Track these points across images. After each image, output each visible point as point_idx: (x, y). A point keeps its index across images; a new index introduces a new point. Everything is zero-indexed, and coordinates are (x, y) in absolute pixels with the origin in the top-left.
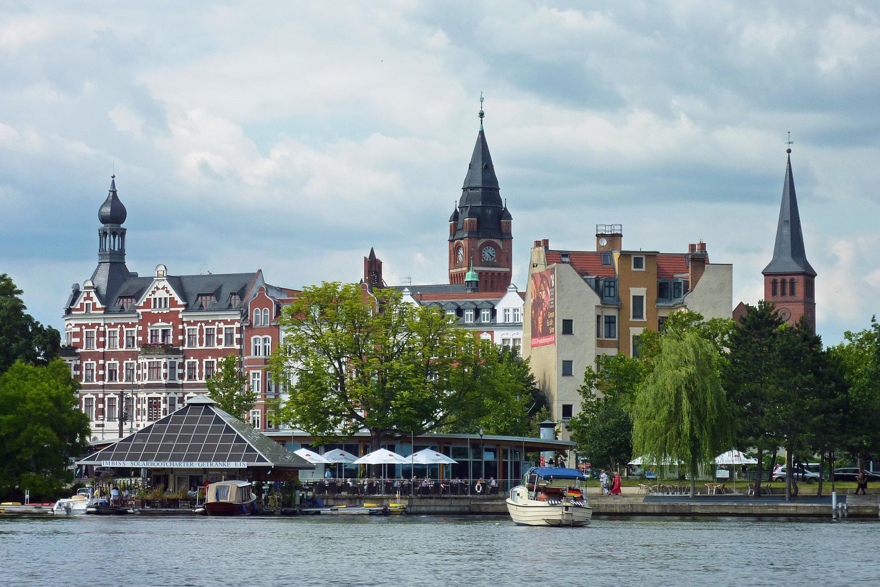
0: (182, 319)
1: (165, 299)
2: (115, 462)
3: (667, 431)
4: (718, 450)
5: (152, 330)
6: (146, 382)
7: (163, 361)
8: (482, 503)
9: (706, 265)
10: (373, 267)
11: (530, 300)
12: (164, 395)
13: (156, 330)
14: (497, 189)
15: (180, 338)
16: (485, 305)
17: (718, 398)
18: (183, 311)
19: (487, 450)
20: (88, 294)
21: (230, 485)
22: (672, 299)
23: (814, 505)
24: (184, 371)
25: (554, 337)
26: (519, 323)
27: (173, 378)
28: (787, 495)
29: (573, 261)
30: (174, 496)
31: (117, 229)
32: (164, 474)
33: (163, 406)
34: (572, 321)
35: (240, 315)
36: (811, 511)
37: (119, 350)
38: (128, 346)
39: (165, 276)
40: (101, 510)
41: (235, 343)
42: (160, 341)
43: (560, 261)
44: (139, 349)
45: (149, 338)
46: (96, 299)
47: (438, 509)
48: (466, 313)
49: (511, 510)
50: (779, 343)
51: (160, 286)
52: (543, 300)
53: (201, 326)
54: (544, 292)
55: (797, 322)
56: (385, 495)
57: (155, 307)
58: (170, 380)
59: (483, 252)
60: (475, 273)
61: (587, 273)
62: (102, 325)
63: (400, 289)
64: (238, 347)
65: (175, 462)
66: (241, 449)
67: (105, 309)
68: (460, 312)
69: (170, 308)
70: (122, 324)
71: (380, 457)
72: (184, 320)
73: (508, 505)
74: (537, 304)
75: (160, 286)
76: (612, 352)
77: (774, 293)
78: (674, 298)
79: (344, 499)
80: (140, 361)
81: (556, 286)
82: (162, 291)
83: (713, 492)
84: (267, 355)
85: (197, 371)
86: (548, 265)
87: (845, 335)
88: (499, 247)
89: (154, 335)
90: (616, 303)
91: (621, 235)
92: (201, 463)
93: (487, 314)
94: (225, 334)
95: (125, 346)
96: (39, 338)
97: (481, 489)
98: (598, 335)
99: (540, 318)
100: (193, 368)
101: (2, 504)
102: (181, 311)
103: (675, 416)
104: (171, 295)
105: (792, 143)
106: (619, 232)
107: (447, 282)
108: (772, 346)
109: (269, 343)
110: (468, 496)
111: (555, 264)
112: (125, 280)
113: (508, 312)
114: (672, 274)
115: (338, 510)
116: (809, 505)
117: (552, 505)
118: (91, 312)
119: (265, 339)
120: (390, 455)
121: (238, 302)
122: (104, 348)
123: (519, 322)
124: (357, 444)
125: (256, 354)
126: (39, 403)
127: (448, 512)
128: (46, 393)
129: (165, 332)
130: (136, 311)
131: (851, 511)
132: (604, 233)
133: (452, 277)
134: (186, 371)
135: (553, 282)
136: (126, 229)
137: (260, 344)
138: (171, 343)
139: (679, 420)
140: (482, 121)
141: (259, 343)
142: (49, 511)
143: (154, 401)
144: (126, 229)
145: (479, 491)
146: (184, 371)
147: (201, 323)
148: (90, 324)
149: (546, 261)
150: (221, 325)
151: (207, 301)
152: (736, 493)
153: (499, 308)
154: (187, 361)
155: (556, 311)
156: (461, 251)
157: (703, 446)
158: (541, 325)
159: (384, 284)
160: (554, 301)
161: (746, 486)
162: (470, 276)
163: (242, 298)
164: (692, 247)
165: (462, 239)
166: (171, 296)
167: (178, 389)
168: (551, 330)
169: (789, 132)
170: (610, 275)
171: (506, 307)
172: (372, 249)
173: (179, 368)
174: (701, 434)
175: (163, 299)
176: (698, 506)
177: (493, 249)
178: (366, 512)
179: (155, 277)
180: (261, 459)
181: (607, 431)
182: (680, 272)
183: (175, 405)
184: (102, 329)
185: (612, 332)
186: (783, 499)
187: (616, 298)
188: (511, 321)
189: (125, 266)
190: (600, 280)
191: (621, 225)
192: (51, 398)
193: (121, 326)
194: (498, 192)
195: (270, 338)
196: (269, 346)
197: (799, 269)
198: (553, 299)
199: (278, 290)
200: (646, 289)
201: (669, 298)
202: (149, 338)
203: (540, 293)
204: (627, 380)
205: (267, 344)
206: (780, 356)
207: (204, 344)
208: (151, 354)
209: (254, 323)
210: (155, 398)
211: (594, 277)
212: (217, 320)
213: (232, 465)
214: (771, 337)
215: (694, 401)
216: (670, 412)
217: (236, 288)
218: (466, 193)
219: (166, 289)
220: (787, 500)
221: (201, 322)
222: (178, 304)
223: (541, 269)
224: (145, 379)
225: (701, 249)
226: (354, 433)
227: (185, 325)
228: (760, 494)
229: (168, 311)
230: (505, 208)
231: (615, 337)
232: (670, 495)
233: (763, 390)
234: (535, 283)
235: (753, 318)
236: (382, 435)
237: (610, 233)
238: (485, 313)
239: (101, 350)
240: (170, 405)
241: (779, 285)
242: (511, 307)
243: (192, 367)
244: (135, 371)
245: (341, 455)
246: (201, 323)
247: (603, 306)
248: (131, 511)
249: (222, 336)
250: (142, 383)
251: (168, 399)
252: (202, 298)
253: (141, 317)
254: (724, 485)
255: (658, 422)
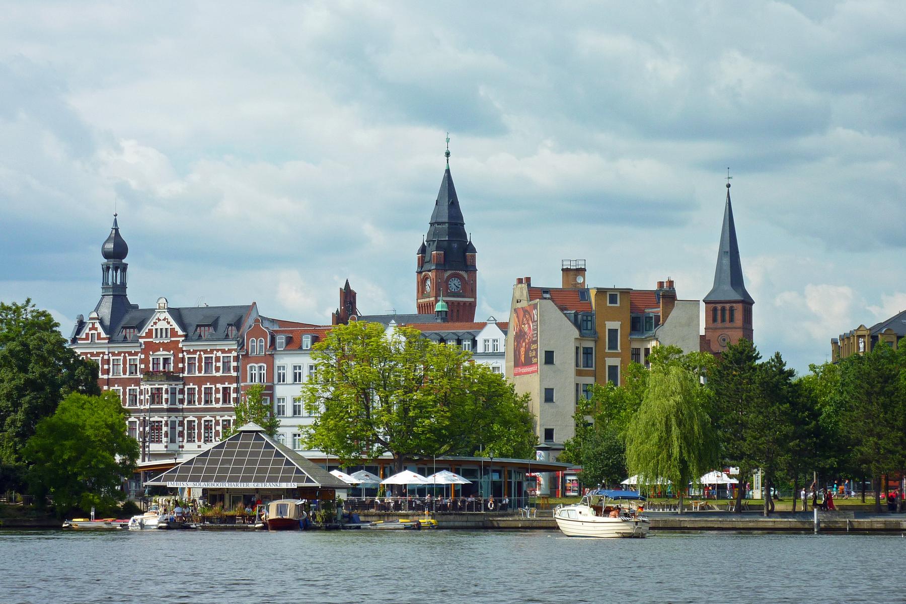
0: (182, 348)
1: (166, 329)
2: (179, 483)
3: (658, 455)
4: (703, 471)
5: (153, 359)
6: (147, 407)
7: (165, 387)
8: (495, 519)
9: (676, 302)
10: (348, 297)
11: (512, 333)
12: (165, 418)
13: (157, 358)
14: (463, 224)
15: (180, 365)
16: (466, 336)
17: (703, 425)
18: (183, 341)
19: (494, 471)
20: (93, 324)
21: (289, 503)
22: (644, 332)
23: (790, 520)
24: (184, 397)
25: (536, 367)
26: (498, 353)
27: (173, 403)
28: (765, 511)
29: (553, 297)
30: (232, 513)
31: (119, 264)
32: (221, 493)
33: (164, 429)
34: (553, 352)
35: (236, 345)
36: (787, 526)
37: (123, 376)
38: (131, 373)
39: (166, 308)
40: (171, 525)
41: (232, 371)
42: (161, 368)
43: (541, 297)
44: (142, 376)
45: (151, 365)
46: (100, 330)
47: (457, 524)
48: (464, 343)
49: (560, 523)
50: (758, 376)
51: (162, 318)
52: (525, 333)
53: (200, 355)
54: (526, 326)
55: (773, 358)
56: (409, 512)
57: (156, 337)
58: (171, 404)
59: (450, 283)
60: (444, 303)
61: (566, 308)
62: (107, 353)
63: (385, 320)
64: (235, 374)
65: (232, 483)
66: (291, 471)
67: (109, 339)
68: (459, 342)
69: (171, 337)
70: (125, 353)
71: (406, 477)
72: (184, 349)
73: (557, 519)
74: (520, 336)
75: (162, 318)
76: (590, 380)
77: (715, 320)
78: (646, 330)
79: (374, 516)
80: (142, 387)
81: (539, 321)
82: (163, 322)
83: (697, 509)
84: (262, 381)
85: (197, 396)
86: (531, 300)
87: (810, 368)
88: (464, 278)
89: (156, 362)
90: (593, 336)
91: (584, 270)
92: (256, 484)
93: (469, 345)
94: (223, 362)
95: (128, 373)
96: (82, 369)
97: (493, 506)
98: (577, 365)
99: (523, 350)
100: (192, 394)
101: (74, 520)
102: (181, 341)
103: (665, 442)
104: (172, 325)
105: (731, 178)
106: (583, 267)
107: (415, 311)
108: (752, 379)
109: (264, 370)
110: (482, 512)
111: (538, 300)
112: (127, 312)
113: (488, 342)
114: (643, 309)
115: (376, 525)
116: (786, 520)
117: (624, 521)
118: (96, 341)
119: (260, 367)
120: (414, 476)
121: (235, 332)
122: (108, 374)
123: (498, 351)
124: (377, 465)
125: (252, 381)
126: (98, 430)
127: (465, 527)
128: (103, 421)
129: (166, 361)
130: (138, 341)
131: (822, 525)
132: (569, 267)
133: (420, 307)
134: (186, 396)
135: (535, 316)
136: (128, 264)
137: (256, 372)
138: (172, 370)
139: (670, 445)
140: (448, 160)
141: (255, 370)
142: (117, 526)
143: (156, 424)
144: (128, 264)
145: (492, 508)
146: (184, 397)
147: (200, 352)
148: (95, 353)
149: (528, 296)
150: (219, 354)
151: (206, 332)
152: (717, 509)
153: (480, 339)
154: (186, 387)
155: (539, 343)
156: (428, 282)
157: (691, 467)
158: (523, 356)
159: (358, 313)
160: (537, 334)
161: (726, 504)
162: (440, 306)
163: (238, 329)
164: (661, 284)
165: (430, 271)
166: (171, 327)
167: (178, 413)
168: (534, 360)
169: (729, 168)
170: (588, 310)
171: (486, 338)
172: (347, 281)
173: (179, 394)
174: (689, 457)
175: (159, 329)
176: (687, 521)
177: (459, 281)
178: (402, 526)
179: (157, 309)
180: (309, 480)
181: (601, 454)
182: (651, 307)
183: (175, 428)
184: (106, 357)
185: (590, 362)
186: (762, 514)
187: (593, 330)
188: (491, 351)
189: (127, 298)
190: (578, 315)
191: (585, 260)
192: (107, 426)
193: (125, 354)
194: (463, 226)
195: (265, 366)
196: (264, 374)
197: (738, 297)
198: (536, 332)
199: (271, 321)
200: (620, 323)
201: (641, 331)
202: (151, 365)
203: (523, 326)
204: (616, 408)
205: (262, 372)
206: (760, 388)
207: (203, 372)
208: (152, 381)
209: (250, 352)
210: (158, 422)
211: (573, 312)
212: (215, 350)
213: (284, 485)
214: (751, 371)
215: (682, 427)
216: (660, 439)
217: (231, 318)
218: (433, 228)
219: (167, 320)
220: (765, 515)
221: (200, 351)
222: (179, 334)
223: (524, 304)
224: (147, 404)
225: (670, 286)
226: (378, 456)
227: (185, 353)
228: (741, 510)
229: (169, 341)
230: (470, 242)
231: (592, 367)
232: (657, 511)
233: (744, 418)
234: (518, 317)
235: (734, 355)
236: (404, 457)
237: (574, 268)
238: (467, 343)
239: (105, 377)
240: (171, 428)
241: (719, 312)
242: (491, 338)
243: (191, 392)
244: (138, 397)
245: (366, 476)
246: (200, 352)
247: (581, 338)
248: (194, 526)
249: (220, 364)
250: (145, 407)
251: (169, 422)
252: (200, 328)
253: (143, 346)
254: (707, 502)
255: (650, 446)
